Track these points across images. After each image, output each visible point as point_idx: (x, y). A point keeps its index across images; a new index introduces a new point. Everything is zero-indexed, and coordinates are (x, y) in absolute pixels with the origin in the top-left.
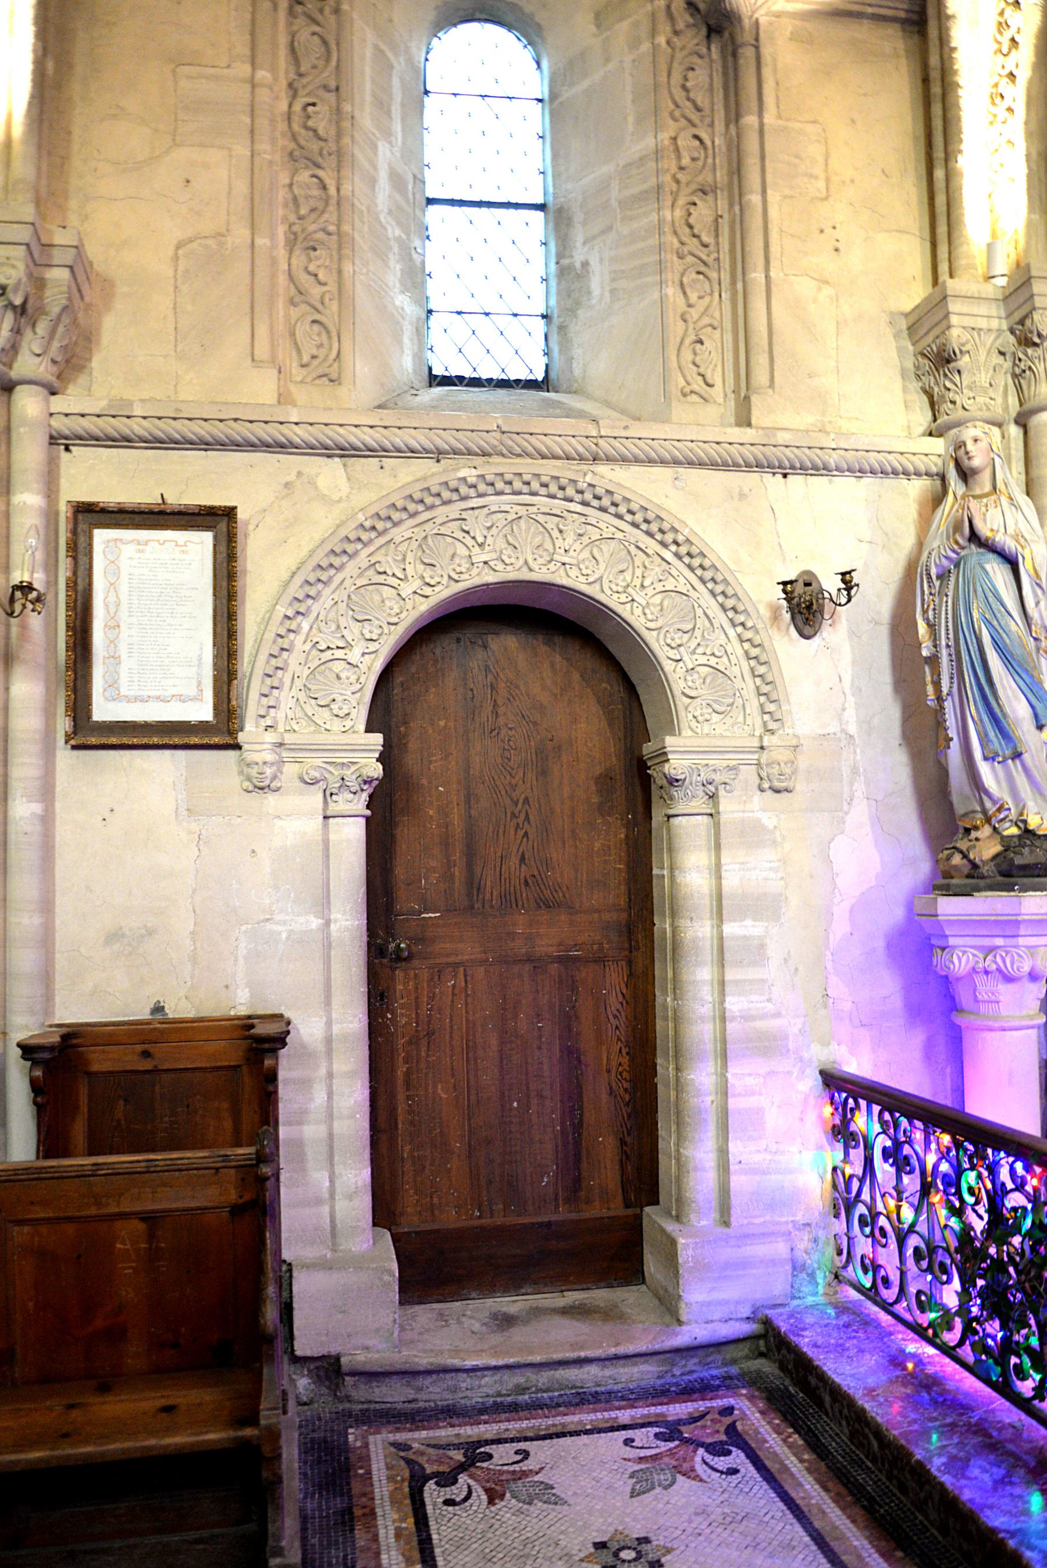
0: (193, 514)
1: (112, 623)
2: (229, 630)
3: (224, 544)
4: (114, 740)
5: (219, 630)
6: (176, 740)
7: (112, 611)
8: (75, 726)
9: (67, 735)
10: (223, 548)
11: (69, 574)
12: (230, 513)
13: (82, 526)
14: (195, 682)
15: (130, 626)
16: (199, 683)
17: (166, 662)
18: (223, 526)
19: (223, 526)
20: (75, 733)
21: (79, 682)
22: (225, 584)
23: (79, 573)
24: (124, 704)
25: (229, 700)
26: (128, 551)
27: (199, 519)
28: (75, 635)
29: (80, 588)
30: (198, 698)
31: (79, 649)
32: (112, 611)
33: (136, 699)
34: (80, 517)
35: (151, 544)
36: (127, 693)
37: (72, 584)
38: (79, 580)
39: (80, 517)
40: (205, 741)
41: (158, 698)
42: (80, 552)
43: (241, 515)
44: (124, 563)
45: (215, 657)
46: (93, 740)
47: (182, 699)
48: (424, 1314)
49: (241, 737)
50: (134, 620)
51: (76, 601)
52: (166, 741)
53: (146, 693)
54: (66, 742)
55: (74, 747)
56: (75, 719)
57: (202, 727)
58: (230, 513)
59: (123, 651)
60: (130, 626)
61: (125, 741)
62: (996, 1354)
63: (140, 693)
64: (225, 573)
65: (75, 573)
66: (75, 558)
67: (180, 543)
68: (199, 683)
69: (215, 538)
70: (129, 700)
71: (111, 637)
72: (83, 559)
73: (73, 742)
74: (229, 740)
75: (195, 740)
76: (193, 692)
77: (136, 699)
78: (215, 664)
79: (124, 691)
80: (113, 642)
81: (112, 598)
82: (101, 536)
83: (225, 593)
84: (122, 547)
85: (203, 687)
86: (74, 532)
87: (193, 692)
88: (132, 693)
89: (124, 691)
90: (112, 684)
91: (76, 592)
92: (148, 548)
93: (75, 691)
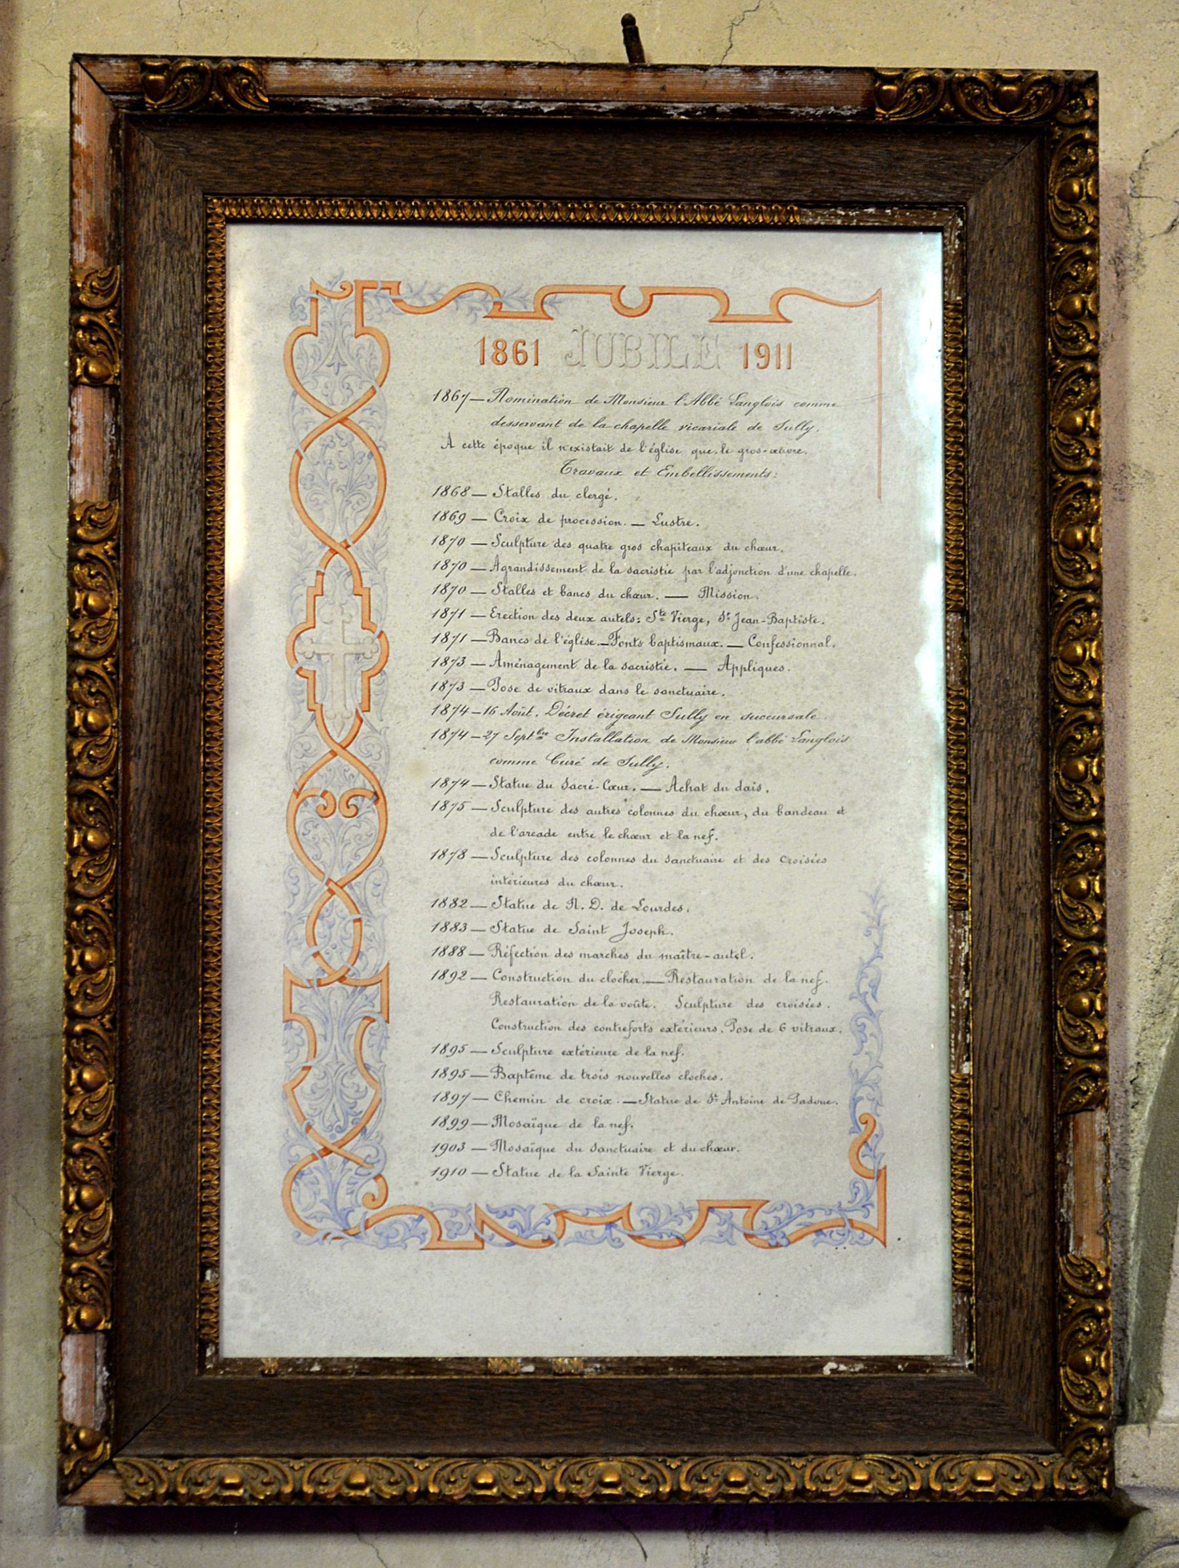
0: (830, 128)
1: (338, 779)
2: (1051, 817)
3: (1018, 302)
4: (357, 1475)
5: (986, 812)
6: (741, 1475)
7: (340, 702)
8: (114, 1391)
9: (69, 1443)
10: (1007, 330)
11: (84, 485)
12: (1047, 119)
13: (162, 209)
14: (836, 1119)
15: (448, 794)
16: (865, 1132)
17: (664, 1003)
18: (1005, 198)
19: (1005, 198)
20: (118, 1430)
21: (140, 1125)
22: (1021, 541)
23: (148, 487)
24: (412, 1256)
25: (1056, 1234)
26: (431, 353)
27: (864, 156)
28: (119, 846)
29: (151, 570)
30: (854, 1223)
31: (141, 944)
32: (340, 702)
33: (484, 1228)
34: (149, 150)
35: (573, 310)
36: (430, 1192)
37: (101, 548)
38: (147, 527)
39: (149, 150)
40: (923, 1476)
41: (615, 1221)
42: (148, 359)
43: (1120, 138)
44: (411, 432)
45: (964, 972)
46: (231, 1476)
47: (762, 1226)
48: (1079, 64)
49: (1139, 1456)
50: (472, 760)
51: (125, 640)
52: (678, 1477)
53: (540, 1193)
54: (65, 1489)
55: (104, 1522)
56: (115, 1354)
57: (874, 1397)
58: (1047, 119)
59: (404, 937)
60: (448, 794)
61: (429, 1476)
62: (1052, 1448)
63: (510, 1192)
64: (1025, 480)
65: (120, 482)
66: (120, 396)
67: (749, 297)
68: (865, 1132)
69: (959, 272)
70: (437, 1231)
71: (336, 858)
72: (162, 405)
73: (104, 1490)
74: (1056, 1473)
75: (863, 1474)
76: (828, 1181)
77: (484, 1228)
78: (961, 1019)
79: (410, 1182)
80: (345, 892)
81: (339, 629)
82: (267, 271)
83: (1026, 592)
84: (400, 330)
85: (889, 1151)
86: (117, 238)
87: (828, 1181)
88: (456, 1192)
89: (410, 1182)
90: (344, 1137)
91: (129, 591)
92: (553, 337)
93: (118, 1175)
